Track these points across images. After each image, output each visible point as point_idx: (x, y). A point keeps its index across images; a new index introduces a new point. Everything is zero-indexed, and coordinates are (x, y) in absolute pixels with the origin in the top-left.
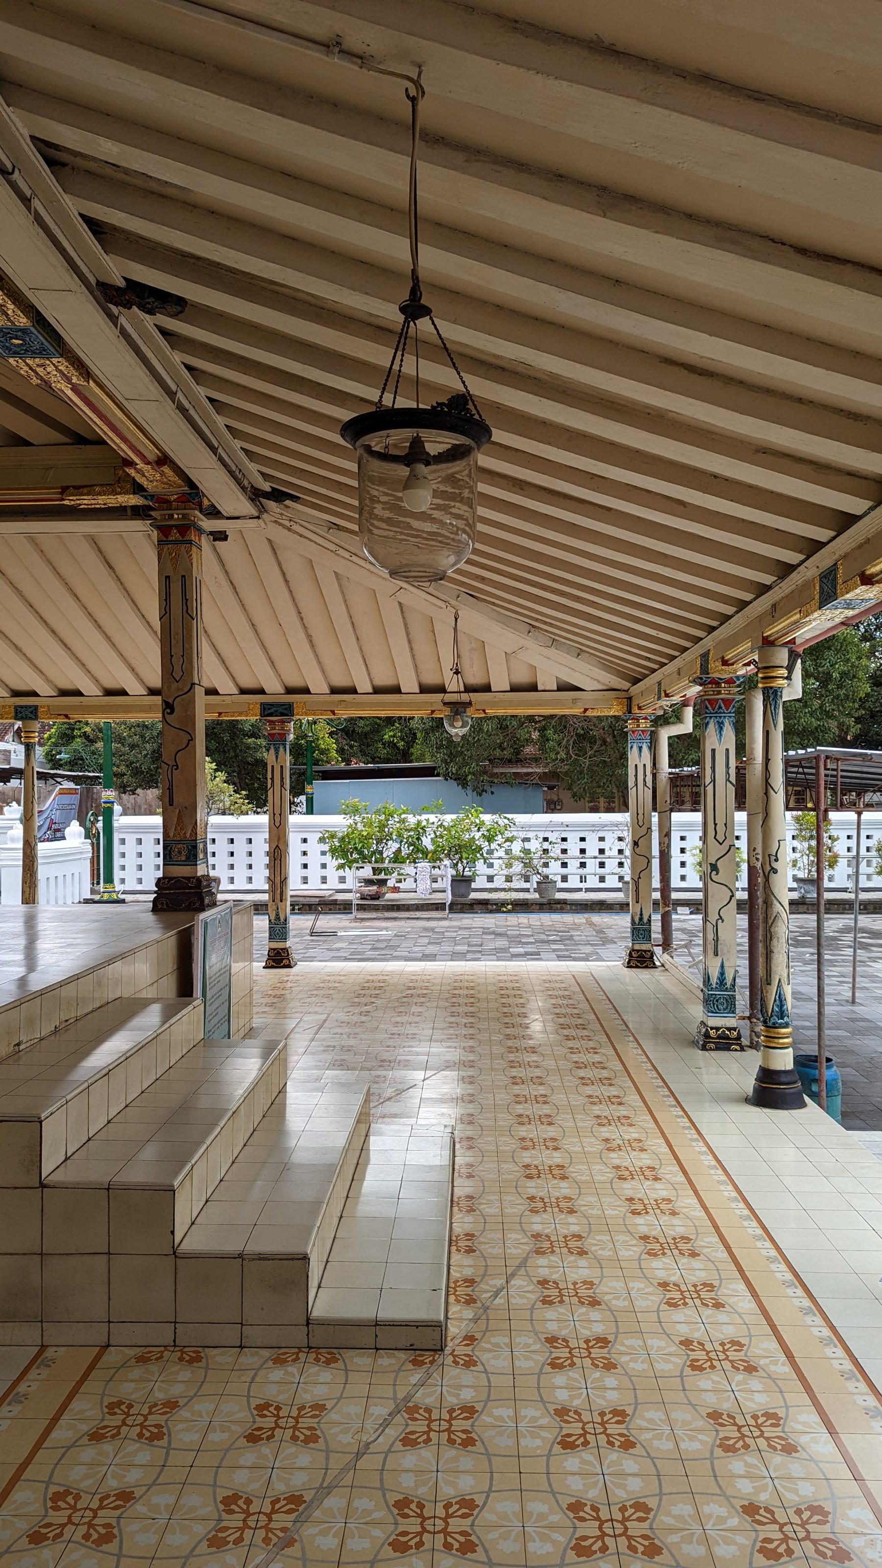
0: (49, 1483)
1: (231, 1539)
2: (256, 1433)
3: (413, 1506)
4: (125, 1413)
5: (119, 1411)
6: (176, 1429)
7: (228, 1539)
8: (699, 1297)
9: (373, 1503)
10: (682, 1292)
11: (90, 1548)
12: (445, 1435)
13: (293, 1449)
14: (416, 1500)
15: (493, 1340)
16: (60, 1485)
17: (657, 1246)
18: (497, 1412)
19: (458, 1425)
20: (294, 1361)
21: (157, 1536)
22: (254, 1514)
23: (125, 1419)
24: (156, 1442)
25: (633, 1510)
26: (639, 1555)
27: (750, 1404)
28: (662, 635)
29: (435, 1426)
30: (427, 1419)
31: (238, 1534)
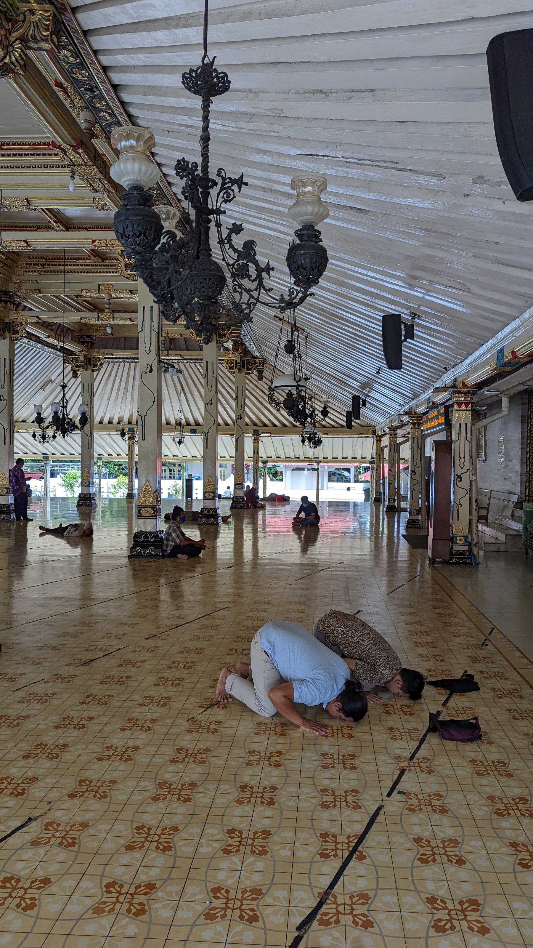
0: (103, 876)
1: (332, 920)
2: (228, 848)
3: (223, 892)
4: (147, 833)
5: (143, 832)
6: (179, 844)
7: (331, 920)
8: (496, 769)
9: (199, 889)
10: (419, 766)
11: (19, 913)
12: (249, 848)
13: (253, 859)
14: (225, 888)
15: (288, 790)
16: (321, 888)
17: (398, 734)
18: (283, 834)
19: (331, 846)
20: (257, 764)
21: (172, 911)
22: (231, 899)
23: (147, 837)
24: (70, 848)
25: (468, 904)
26: (475, 933)
27: (458, 892)
28: (433, 365)
29: (244, 842)
30: (334, 842)
31: (223, 912)
